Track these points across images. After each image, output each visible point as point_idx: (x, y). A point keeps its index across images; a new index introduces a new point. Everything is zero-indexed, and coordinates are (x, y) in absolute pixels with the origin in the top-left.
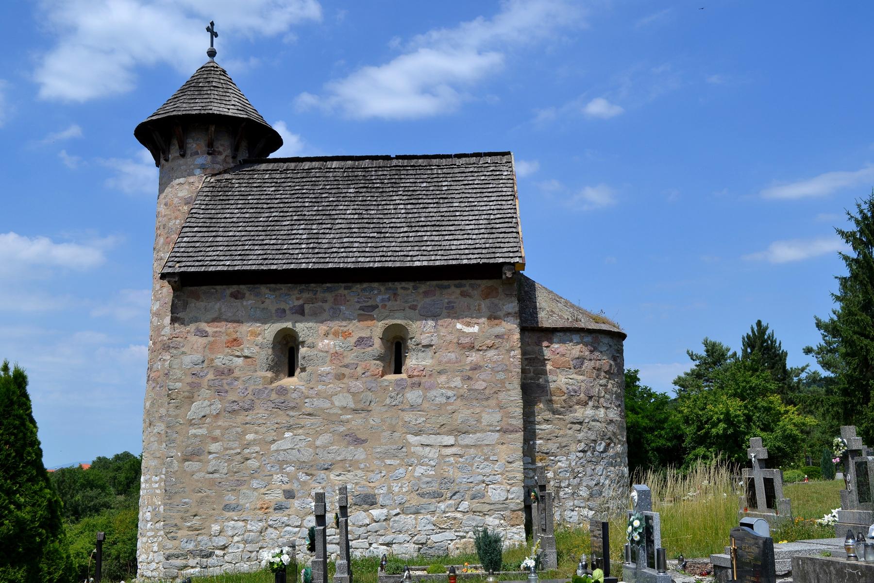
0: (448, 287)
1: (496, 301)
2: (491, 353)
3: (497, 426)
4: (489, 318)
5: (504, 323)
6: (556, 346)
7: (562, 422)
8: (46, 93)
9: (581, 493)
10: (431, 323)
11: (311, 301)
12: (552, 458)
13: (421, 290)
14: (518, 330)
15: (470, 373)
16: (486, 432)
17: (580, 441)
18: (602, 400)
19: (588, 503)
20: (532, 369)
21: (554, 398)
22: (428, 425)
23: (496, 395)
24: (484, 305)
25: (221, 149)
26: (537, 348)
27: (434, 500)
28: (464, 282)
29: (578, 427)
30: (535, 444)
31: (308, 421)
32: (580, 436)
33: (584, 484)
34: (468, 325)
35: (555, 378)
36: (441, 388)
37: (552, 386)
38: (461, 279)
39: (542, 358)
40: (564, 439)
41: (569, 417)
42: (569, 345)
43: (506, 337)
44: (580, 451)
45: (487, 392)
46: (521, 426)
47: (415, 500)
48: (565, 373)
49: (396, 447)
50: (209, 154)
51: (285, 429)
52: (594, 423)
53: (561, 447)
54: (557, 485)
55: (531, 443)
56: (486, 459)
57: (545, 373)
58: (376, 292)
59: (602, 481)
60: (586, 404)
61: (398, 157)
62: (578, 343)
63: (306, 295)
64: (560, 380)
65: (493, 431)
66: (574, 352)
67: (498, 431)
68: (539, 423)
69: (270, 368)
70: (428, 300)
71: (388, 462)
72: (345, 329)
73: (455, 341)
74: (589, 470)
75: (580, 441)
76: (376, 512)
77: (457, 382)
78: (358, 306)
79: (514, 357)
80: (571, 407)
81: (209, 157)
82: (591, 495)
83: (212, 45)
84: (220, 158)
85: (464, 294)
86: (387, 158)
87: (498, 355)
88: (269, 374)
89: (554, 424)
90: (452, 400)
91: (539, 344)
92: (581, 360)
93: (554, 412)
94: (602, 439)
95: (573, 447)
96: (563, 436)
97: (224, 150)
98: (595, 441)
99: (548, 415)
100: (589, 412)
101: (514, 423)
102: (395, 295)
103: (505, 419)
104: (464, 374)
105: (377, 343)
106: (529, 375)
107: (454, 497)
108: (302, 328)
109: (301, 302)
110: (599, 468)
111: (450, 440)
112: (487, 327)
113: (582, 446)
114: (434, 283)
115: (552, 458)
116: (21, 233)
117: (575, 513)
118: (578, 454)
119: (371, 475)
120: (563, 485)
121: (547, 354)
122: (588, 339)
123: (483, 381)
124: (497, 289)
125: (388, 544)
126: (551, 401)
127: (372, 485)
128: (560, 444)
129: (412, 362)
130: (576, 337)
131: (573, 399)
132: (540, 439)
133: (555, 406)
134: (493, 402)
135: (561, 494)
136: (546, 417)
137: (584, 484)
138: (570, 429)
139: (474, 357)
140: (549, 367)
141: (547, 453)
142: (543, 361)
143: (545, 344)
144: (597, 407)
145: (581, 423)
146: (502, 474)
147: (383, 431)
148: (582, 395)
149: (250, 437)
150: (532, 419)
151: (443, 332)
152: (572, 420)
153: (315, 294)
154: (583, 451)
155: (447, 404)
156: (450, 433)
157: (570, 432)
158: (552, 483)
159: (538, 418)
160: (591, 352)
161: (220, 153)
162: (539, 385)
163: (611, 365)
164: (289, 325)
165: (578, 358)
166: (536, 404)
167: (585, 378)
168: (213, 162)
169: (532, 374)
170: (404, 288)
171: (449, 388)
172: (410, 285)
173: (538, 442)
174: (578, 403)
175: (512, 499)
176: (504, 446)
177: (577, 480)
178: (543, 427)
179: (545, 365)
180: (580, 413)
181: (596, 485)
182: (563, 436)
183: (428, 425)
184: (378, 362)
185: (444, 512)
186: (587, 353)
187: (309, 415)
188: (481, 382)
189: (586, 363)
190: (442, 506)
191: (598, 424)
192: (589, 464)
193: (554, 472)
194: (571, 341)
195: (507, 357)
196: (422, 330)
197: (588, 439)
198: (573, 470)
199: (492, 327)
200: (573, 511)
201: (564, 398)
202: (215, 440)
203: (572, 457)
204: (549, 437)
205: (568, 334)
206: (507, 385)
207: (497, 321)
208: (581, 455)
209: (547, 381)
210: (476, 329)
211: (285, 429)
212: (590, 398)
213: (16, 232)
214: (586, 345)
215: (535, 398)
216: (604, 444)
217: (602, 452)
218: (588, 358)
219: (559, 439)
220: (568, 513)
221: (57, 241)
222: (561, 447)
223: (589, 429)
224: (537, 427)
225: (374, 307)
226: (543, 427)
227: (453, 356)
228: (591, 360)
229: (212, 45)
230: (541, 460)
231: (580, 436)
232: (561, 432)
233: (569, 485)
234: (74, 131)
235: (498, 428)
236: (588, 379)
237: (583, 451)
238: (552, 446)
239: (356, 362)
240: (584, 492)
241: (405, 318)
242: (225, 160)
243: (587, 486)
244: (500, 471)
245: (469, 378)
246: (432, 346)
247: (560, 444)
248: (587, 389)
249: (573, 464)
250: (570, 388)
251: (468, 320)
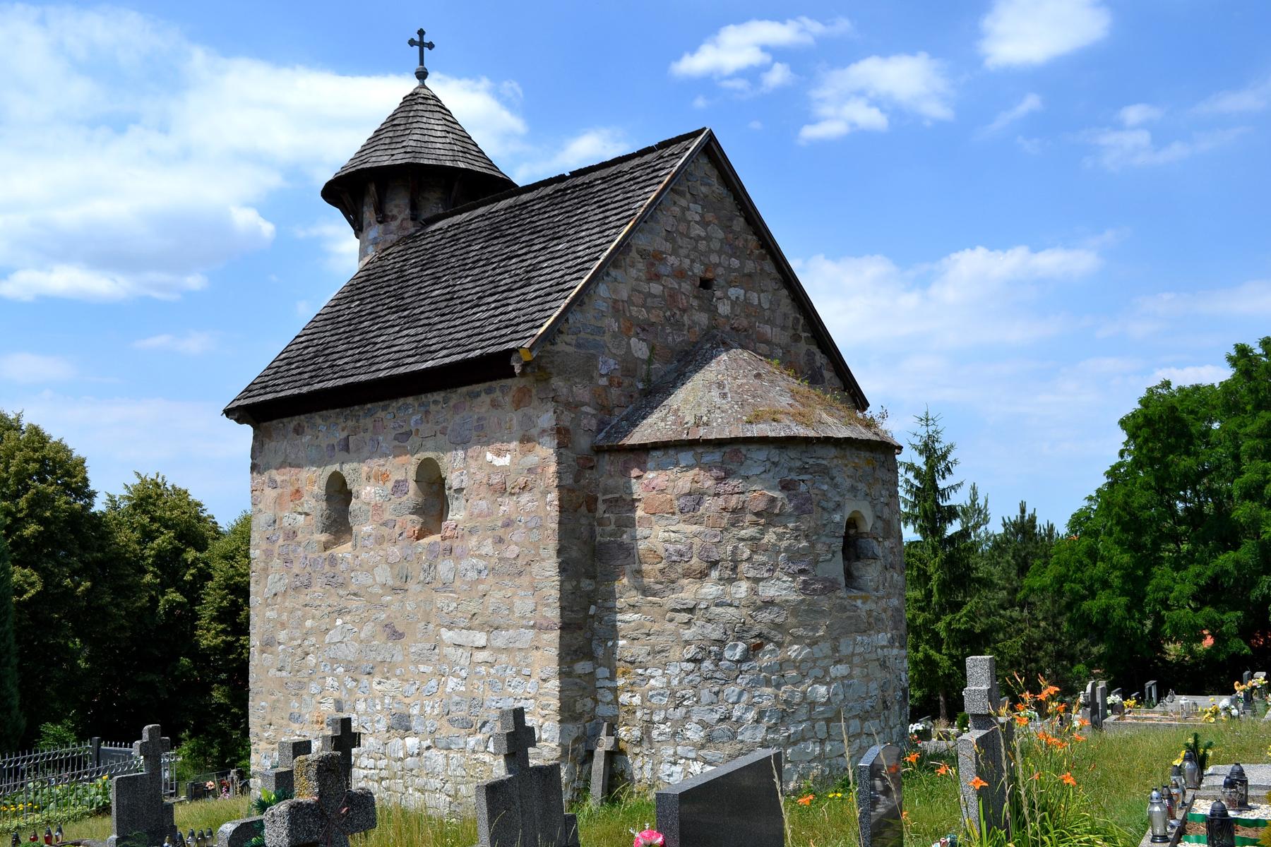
0: (478, 395)
1: (529, 411)
2: (525, 498)
3: (530, 619)
4: (522, 441)
5: (538, 447)
6: (650, 475)
7: (657, 609)
8: (990, 63)
9: (689, 734)
10: (461, 453)
11: (355, 431)
12: (640, 671)
13: (451, 404)
14: (554, 458)
15: (500, 532)
16: (518, 628)
17: (688, 643)
18: (743, 567)
19: (701, 753)
20: (613, 517)
21: (645, 567)
22: (460, 614)
23: (528, 568)
24: (515, 418)
25: (395, 212)
26: (622, 481)
27: (463, 732)
28: (494, 384)
29: (685, 617)
30: (615, 645)
31: (354, 604)
32: (688, 634)
33: (695, 719)
34: (499, 454)
35: (646, 532)
36: (472, 556)
37: (642, 546)
38: (491, 380)
39: (628, 498)
40: (661, 639)
41: (671, 600)
42: (672, 473)
43: (539, 471)
44: (688, 661)
45: (520, 562)
46: (557, 620)
47: (447, 731)
48: (665, 522)
49: (428, 646)
50: (380, 222)
51: (336, 614)
52: (720, 610)
53: (653, 652)
54: (646, 718)
55: (610, 643)
56: (518, 673)
57: (631, 523)
58: (411, 411)
59: (736, 713)
60: (703, 575)
61: (575, 174)
62: (689, 467)
63: (350, 423)
64: (656, 535)
65: (527, 627)
66: (680, 483)
67: (533, 627)
68: (621, 611)
69: (326, 529)
70: (457, 418)
71: (422, 668)
72: (382, 469)
73: (484, 481)
74: (706, 695)
75: (688, 643)
76: (411, 742)
77: (488, 548)
78: (394, 433)
79: (550, 503)
80: (673, 582)
81: (381, 226)
82: (710, 739)
83: (422, 63)
84: (394, 225)
85: (495, 405)
86: (561, 178)
87: (533, 501)
88: (324, 537)
89: (644, 613)
90: (483, 576)
91: (625, 473)
92: (697, 497)
93: (645, 591)
94: (739, 639)
95: (675, 653)
96: (659, 633)
97: (400, 212)
98: (721, 643)
99: (635, 597)
100: (710, 589)
101: (549, 615)
102: (427, 412)
103: (539, 607)
104: (496, 533)
105: (412, 486)
106: (608, 529)
107: (484, 730)
108: (347, 470)
109: (345, 434)
110: (731, 691)
111: (480, 638)
112: (519, 456)
113: (692, 651)
114: (464, 389)
115: (640, 671)
116: (991, 247)
117: (678, 769)
118: (684, 665)
119: (407, 686)
120: (656, 718)
121: (638, 489)
122: (716, 456)
123: (516, 544)
124: (529, 391)
125: (422, 791)
126: (639, 572)
127: (407, 701)
128: (653, 647)
129: (457, 514)
130: (686, 457)
131: (679, 567)
132: (624, 637)
133: (646, 580)
134: (525, 580)
135: (655, 733)
136: (632, 601)
137: (695, 719)
138: (671, 620)
139: (507, 506)
140: (639, 513)
141: (632, 663)
142: (632, 504)
143: (635, 472)
144: (731, 581)
145: (691, 610)
146: (534, 698)
147: (418, 622)
148: (695, 560)
149: (309, 623)
150: (610, 604)
151: (474, 466)
152: (673, 605)
153: (358, 421)
154: (693, 660)
155: (479, 581)
156: (481, 628)
157: (671, 626)
158: (639, 714)
159: (620, 603)
160: (719, 480)
161: (394, 218)
162: (621, 545)
163: (21, 592)
164: (336, 467)
165: (689, 494)
166: (616, 578)
167: (702, 528)
168: (386, 233)
169: (613, 527)
170: (435, 402)
171: (480, 556)
172: (439, 396)
173: (621, 643)
174: (686, 575)
175: (546, 740)
176: (540, 652)
177: (681, 712)
178: (627, 617)
179: (633, 509)
180: (689, 592)
181: (720, 720)
182: (659, 633)
183: (460, 614)
184: (414, 517)
185: (474, 752)
186: (709, 483)
187: (355, 595)
188: (512, 547)
189: (708, 502)
190: (472, 741)
191: (731, 610)
192: (708, 684)
193: (642, 696)
194: (677, 464)
195: (542, 503)
196: (457, 468)
197: (705, 638)
198: (673, 694)
199: (525, 455)
200: (675, 763)
201: (661, 566)
202: (283, 626)
203: (673, 670)
204: (634, 635)
205: (672, 452)
206: (541, 551)
207: (530, 445)
208: (691, 666)
209: (634, 539)
210: (505, 461)
211: (336, 614)
212: (714, 564)
213: (986, 247)
214: (707, 468)
215: (616, 567)
216: (741, 646)
217: (738, 661)
218: (712, 492)
219: (653, 639)
220: (665, 768)
221: (1036, 249)
222: (653, 652)
223: (709, 621)
224: (619, 617)
225: (408, 434)
226: (627, 617)
227: (483, 504)
228: (718, 495)
229: (422, 63)
230: (624, 673)
231: (688, 634)
232: (656, 627)
233: (665, 720)
234: (1032, 102)
235: (532, 623)
236: (708, 531)
237: (693, 660)
238: (639, 651)
239: (393, 517)
240: (694, 733)
241: (435, 450)
242: (401, 227)
243: (701, 722)
244: (533, 692)
245: (501, 540)
246: (462, 489)
247: (653, 647)
248: (703, 548)
249: (675, 682)
250: (671, 548)
251: (498, 445)
